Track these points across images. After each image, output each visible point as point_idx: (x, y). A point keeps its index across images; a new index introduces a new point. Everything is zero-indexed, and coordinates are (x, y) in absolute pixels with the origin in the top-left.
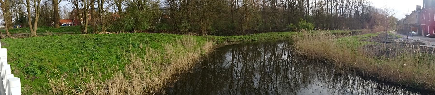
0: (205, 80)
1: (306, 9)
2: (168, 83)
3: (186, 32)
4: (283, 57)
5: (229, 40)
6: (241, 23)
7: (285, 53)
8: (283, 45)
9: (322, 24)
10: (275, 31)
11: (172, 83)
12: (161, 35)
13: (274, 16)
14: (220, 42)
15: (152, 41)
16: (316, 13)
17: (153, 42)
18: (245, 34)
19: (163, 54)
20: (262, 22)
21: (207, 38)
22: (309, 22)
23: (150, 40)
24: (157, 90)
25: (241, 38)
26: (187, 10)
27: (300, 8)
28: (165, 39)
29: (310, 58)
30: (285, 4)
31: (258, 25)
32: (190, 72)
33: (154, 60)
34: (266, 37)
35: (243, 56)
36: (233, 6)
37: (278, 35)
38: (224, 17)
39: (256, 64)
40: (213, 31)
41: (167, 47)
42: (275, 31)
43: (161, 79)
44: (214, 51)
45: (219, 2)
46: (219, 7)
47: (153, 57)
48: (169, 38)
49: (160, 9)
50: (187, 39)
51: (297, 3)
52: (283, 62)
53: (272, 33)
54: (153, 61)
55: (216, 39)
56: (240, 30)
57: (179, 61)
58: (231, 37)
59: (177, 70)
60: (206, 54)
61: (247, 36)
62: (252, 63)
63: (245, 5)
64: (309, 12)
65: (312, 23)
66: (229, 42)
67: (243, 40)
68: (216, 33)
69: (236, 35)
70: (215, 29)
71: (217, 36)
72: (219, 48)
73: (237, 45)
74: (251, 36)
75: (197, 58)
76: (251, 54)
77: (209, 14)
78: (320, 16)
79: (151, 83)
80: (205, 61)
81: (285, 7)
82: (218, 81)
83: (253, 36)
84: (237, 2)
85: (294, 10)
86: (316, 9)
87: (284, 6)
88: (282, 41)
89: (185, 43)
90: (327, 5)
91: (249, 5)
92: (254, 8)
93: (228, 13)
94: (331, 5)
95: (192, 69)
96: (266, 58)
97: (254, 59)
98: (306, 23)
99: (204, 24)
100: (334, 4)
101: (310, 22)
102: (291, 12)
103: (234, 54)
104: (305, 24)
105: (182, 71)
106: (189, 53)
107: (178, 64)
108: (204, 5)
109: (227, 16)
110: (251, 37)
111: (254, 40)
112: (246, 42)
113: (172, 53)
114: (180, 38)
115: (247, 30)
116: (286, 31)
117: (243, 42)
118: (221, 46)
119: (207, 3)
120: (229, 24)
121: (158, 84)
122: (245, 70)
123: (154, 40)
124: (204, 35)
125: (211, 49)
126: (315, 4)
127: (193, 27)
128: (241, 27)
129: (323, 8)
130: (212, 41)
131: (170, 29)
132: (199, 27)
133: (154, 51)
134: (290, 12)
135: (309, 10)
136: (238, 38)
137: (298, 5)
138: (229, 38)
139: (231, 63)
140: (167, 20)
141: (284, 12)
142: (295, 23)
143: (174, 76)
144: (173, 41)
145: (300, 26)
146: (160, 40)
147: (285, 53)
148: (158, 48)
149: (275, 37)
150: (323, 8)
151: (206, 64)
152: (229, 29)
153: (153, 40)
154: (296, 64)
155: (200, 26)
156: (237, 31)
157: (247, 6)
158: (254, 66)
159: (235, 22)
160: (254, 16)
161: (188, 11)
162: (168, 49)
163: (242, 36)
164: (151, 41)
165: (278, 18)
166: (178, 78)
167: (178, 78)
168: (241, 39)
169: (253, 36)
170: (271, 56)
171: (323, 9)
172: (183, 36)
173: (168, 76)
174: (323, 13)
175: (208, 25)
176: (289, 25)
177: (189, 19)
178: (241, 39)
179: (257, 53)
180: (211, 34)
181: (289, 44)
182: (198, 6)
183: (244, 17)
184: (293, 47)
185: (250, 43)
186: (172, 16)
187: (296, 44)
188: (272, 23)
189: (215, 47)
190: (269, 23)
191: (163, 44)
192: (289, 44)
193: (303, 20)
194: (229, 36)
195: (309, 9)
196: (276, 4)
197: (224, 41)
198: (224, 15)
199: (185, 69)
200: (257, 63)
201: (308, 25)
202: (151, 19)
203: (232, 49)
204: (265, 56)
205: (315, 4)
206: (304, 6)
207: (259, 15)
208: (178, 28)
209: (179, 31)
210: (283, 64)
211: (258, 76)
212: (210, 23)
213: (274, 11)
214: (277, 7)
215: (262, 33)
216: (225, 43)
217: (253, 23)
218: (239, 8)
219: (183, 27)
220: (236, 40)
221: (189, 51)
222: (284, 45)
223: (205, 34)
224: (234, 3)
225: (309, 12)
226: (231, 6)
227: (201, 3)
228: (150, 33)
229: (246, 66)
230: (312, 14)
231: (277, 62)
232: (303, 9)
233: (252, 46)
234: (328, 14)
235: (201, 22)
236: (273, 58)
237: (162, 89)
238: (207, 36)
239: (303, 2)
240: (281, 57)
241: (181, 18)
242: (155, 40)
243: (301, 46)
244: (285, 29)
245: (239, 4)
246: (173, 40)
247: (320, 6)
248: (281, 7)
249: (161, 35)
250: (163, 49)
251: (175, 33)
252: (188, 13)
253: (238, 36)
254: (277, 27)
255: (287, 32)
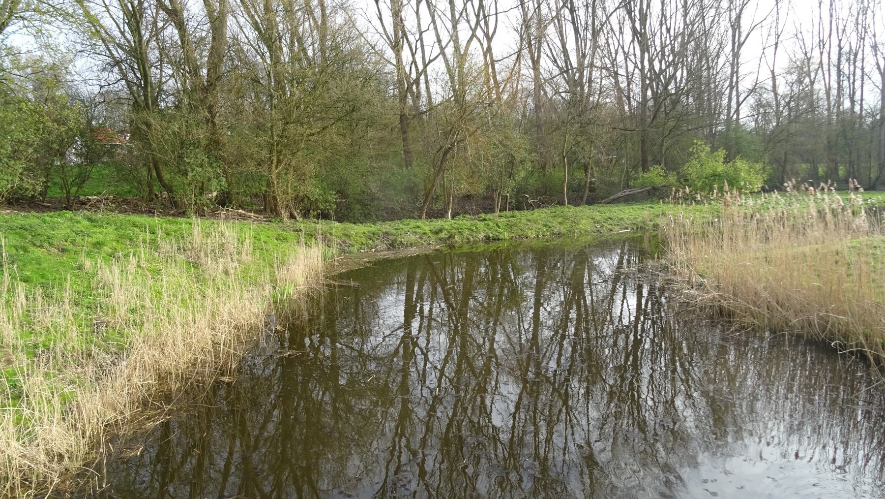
0: (296, 409)
1: (725, 101)
2: (113, 438)
3: (205, 208)
4: (616, 311)
5: (392, 238)
6: (440, 170)
7: (624, 297)
8: (616, 262)
9: (804, 166)
10: (582, 198)
11: (132, 441)
12: (78, 222)
13: (579, 139)
14: (353, 246)
15: (31, 248)
16: (778, 114)
17: (38, 252)
18: (458, 214)
19: (88, 308)
20: (528, 165)
21: (300, 233)
22: (742, 158)
23: (16, 248)
24: (56, 480)
25: (441, 230)
26: (210, 112)
27: (699, 98)
28: (100, 238)
29: (748, 320)
30: (629, 85)
31: (511, 176)
32: (226, 379)
33: (41, 339)
34: (545, 226)
35: (449, 305)
36: (410, 101)
37: (598, 218)
38: (370, 144)
39: (500, 338)
40: (326, 201)
41: (111, 274)
42: (585, 199)
43: (79, 425)
44: (329, 285)
45: (348, 82)
46: (350, 104)
47: (37, 328)
48: (122, 232)
49: (75, 97)
50: (208, 235)
51: (682, 77)
52: (617, 332)
53: (570, 210)
54: (36, 346)
55: (339, 234)
56: (437, 199)
57: (174, 334)
58: (401, 226)
59: (162, 377)
60: (295, 297)
61: (465, 222)
62: (487, 330)
63: (459, 96)
64: (737, 111)
65: (757, 162)
66: (392, 246)
67: (451, 236)
68: (335, 212)
69: (420, 218)
70: (334, 192)
71: (340, 220)
72: (352, 271)
73: (427, 261)
74: (485, 220)
75: (257, 316)
76: (481, 295)
77: (309, 131)
78: (794, 128)
79: (23, 456)
80: (293, 328)
81: (628, 98)
82: (349, 409)
83: (490, 223)
84: (427, 82)
85: (668, 109)
86: (776, 94)
87: (622, 95)
88: (614, 243)
89: (202, 253)
90: (839, 71)
91: (474, 93)
92: (495, 107)
93: (386, 125)
94: (859, 73)
95: (233, 367)
96: (542, 313)
97: (493, 314)
98: (728, 160)
99: (286, 174)
100: (878, 64)
101: (745, 156)
102: (655, 117)
103: (415, 296)
104: (720, 168)
105: (187, 379)
106: (218, 297)
107: (168, 350)
108: (284, 93)
109: (381, 141)
110: (481, 225)
111: (497, 239)
112: (461, 247)
113: (135, 303)
114: (175, 231)
115: (468, 197)
116: (629, 200)
117: (451, 247)
118: (359, 264)
119: (298, 83)
120: (393, 174)
121: (63, 451)
122: (456, 362)
123: (41, 247)
124: (285, 219)
125: (319, 278)
126: (773, 72)
127: (238, 183)
128: (442, 186)
129: (816, 86)
130: (321, 247)
131: (129, 192)
132: (264, 183)
133: (40, 299)
134: (649, 120)
135: (739, 104)
136: (427, 231)
137: (686, 84)
138: (394, 231)
139: (400, 333)
140: (110, 153)
141: (623, 119)
142: (672, 165)
143: (145, 404)
144: (142, 250)
145: (694, 176)
146: (73, 242)
147: (624, 297)
148: (60, 284)
149: (585, 224)
150: (812, 91)
151: (296, 341)
152: (393, 193)
153: (35, 245)
154: (675, 348)
155: (268, 180)
156: (425, 202)
157: (468, 98)
158: (495, 346)
159: (419, 165)
160: (497, 137)
161: (213, 117)
162: (117, 282)
163: (447, 223)
164: (26, 250)
165: (596, 147)
166: (167, 408)
167: (167, 408)
168: (443, 235)
169: (490, 220)
170: (567, 305)
171: (812, 95)
172: (190, 224)
173: (115, 410)
174: (813, 111)
175: (301, 177)
176: (645, 175)
177: (220, 152)
178: (443, 235)
179: (506, 291)
180: (318, 214)
181: (643, 255)
182: (257, 96)
183: (453, 145)
184: (665, 269)
185: (479, 250)
186: (139, 133)
187: (678, 253)
188: (570, 165)
189: (333, 267)
190: (557, 169)
191: (88, 264)
192: (643, 255)
193: (708, 149)
194: (392, 223)
195: (741, 99)
196: (590, 86)
197: (371, 242)
198: (371, 133)
199: (203, 366)
200: (508, 331)
201: (736, 170)
202: (21, 142)
203: (403, 278)
204: (538, 305)
205: (773, 72)
206: (716, 87)
207: (516, 135)
208: (170, 190)
209: (175, 204)
210: (615, 343)
211: (510, 389)
212: (310, 168)
213: (580, 115)
214: (591, 99)
215: (530, 207)
216: (376, 251)
217: (491, 166)
218: (431, 108)
219: (190, 184)
220: (420, 238)
221: (218, 289)
222: (620, 262)
223: (292, 216)
224: (414, 87)
225: (741, 112)
226: (398, 99)
227: (270, 83)
228: (23, 209)
229: (463, 346)
230: (756, 121)
231: (592, 331)
232: (709, 100)
233: (488, 263)
234: (844, 112)
235: (274, 165)
236: (573, 315)
237: (81, 474)
238: (303, 224)
239: (709, 68)
240: (609, 311)
241: (183, 144)
242: (46, 245)
243: (701, 267)
244: (628, 192)
245: (433, 87)
246: (144, 242)
247: (800, 82)
248: (608, 100)
249: (78, 222)
250: (89, 287)
251: (150, 212)
252: (213, 122)
253: (428, 223)
254: (591, 183)
255: (635, 207)
